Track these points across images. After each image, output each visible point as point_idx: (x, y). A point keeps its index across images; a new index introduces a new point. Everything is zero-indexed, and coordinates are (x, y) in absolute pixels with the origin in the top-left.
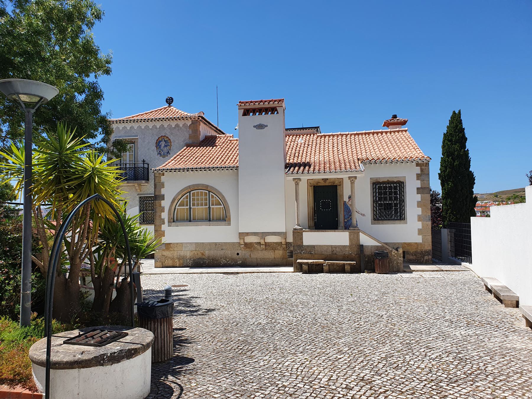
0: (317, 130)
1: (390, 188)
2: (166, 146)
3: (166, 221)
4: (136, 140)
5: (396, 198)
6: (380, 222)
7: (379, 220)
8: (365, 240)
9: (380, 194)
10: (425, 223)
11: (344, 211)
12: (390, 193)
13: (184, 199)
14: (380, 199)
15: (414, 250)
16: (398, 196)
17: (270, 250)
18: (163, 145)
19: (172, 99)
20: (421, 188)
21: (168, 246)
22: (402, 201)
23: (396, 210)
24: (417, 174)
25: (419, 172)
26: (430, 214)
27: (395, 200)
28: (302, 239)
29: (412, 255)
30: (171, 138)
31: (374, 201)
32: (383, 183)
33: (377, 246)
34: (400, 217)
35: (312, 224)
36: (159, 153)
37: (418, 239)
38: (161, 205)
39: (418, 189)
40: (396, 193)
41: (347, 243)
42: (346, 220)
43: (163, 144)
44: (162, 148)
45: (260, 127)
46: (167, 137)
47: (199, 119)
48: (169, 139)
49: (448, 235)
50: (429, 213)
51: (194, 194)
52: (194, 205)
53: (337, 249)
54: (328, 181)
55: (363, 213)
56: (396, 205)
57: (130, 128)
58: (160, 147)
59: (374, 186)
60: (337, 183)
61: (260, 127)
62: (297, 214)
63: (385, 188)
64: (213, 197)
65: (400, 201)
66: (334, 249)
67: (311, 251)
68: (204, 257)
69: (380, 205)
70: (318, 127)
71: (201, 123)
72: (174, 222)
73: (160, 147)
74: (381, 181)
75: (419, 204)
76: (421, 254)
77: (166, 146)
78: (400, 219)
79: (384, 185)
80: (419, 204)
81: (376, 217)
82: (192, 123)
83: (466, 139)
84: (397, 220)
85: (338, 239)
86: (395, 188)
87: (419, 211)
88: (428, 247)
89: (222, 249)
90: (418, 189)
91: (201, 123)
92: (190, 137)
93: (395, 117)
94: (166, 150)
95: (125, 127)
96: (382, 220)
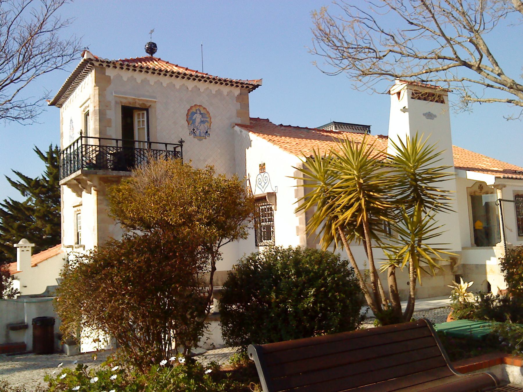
2: (202, 122)
4: (153, 105)
18: (198, 120)
19: (155, 45)
30: (210, 109)
36: (193, 132)
41: (90, 200)
43: (198, 118)
44: (197, 124)
46: (204, 108)
48: (208, 112)
57: (142, 81)
70: (369, 126)
73: (194, 121)
76: (217, 251)
77: (202, 122)
82: (240, 94)
83: (267, 120)
94: (203, 128)
95: (133, 79)
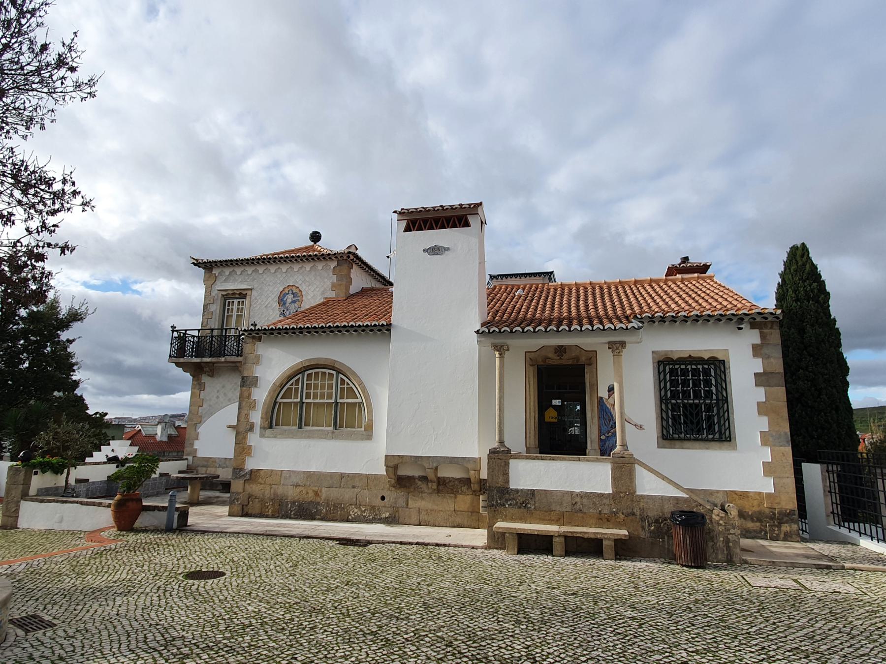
0: (550, 279)
1: (695, 372)
3: (257, 428)
5: (709, 394)
6: (678, 443)
7: (673, 439)
8: (648, 485)
9: (674, 383)
10: (777, 448)
11: (599, 418)
12: (696, 384)
13: (292, 384)
14: (674, 395)
15: (756, 509)
16: (714, 389)
17: (447, 492)
18: (289, 301)
20: (765, 373)
21: (254, 475)
22: (724, 401)
23: (710, 418)
24: (753, 345)
25: (757, 340)
26: (788, 430)
27: (706, 397)
28: (506, 474)
29: (753, 521)
31: (662, 400)
32: (681, 361)
33: (677, 499)
34: (721, 434)
35: (534, 441)
37: (767, 486)
38: (250, 395)
39: (756, 375)
40: (708, 383)
42: (603, 437)
45: (435, 250)
47: (349, 257)
49: (824, 480)
50: (786, 428)
51: (309, 376)
52: (308, 397)
53: (585, 501)
54: (565, 356)
55: (639, 423)
56: (709, 408)
58: (285, 304)
59: (661, 369)
60: (583, 359)
61: (435, 250)
62: (500, 419)
63: (685, 372)
64: (343, 381)
65: (717, 399)
66: (578, 499)
67: (528, 502)
68: (318, 499)
69: (675, 408)
70: (552, 272)
71: (354, 266)
72: (271, 427)
74: (675, 357)
75: (762, 408)
77: (294, 302)
78: (720, 440)
79: (683, 367)
80: (762, 408)
81: (668, 432)
84: (713, 440)
85: (589, 476)
86: (707, 372)
87: (764, 424)
88: (789, 503)
89: (354, 487)
90: (756, 375)
91: (354, 266)
92: (334, 287)
93: (685, 259)
96: (680, 439)
